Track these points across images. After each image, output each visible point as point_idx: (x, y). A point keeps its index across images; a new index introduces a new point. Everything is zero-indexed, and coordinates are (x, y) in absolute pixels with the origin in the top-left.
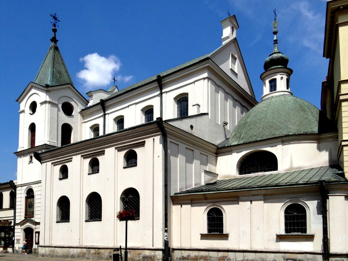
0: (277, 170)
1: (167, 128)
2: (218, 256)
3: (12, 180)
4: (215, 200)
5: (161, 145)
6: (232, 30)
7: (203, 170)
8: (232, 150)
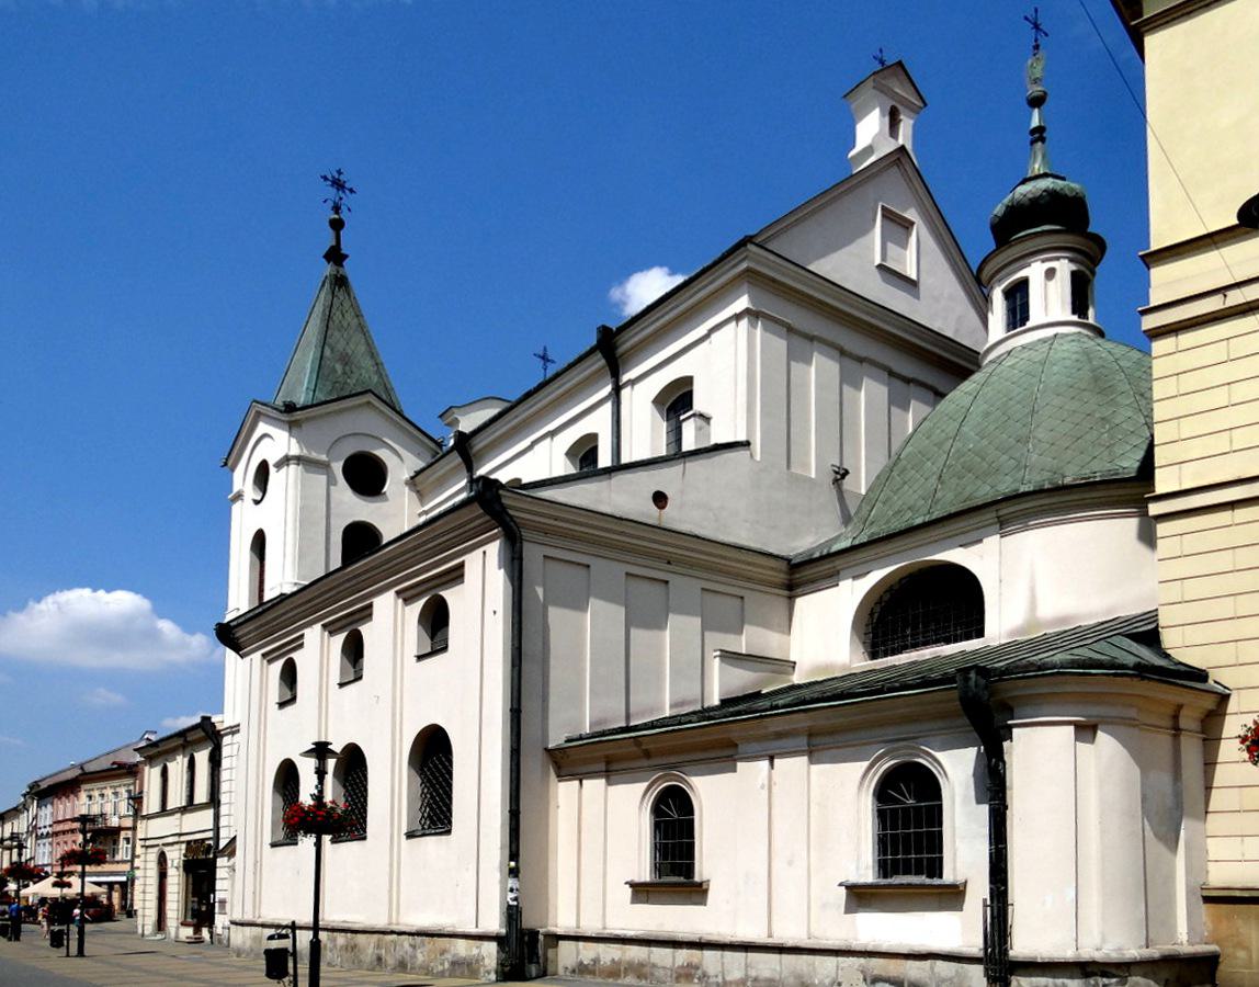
1: (517, 509)
3: (209, 715)
4: (673, 759)
5: (502, 570)
6: (887, 119)
7: (715, 651)
8: (839, 568)
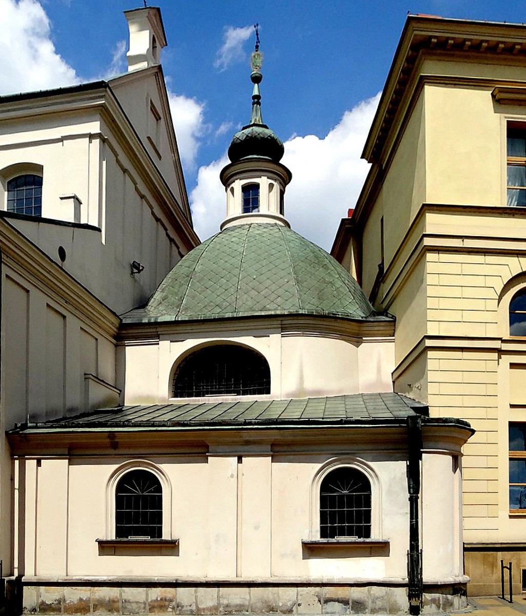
0: (268, 392)
2: (147, 599)
